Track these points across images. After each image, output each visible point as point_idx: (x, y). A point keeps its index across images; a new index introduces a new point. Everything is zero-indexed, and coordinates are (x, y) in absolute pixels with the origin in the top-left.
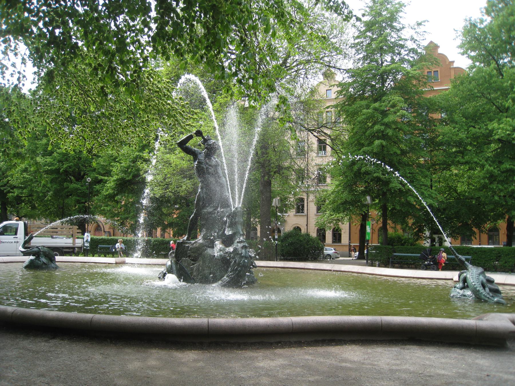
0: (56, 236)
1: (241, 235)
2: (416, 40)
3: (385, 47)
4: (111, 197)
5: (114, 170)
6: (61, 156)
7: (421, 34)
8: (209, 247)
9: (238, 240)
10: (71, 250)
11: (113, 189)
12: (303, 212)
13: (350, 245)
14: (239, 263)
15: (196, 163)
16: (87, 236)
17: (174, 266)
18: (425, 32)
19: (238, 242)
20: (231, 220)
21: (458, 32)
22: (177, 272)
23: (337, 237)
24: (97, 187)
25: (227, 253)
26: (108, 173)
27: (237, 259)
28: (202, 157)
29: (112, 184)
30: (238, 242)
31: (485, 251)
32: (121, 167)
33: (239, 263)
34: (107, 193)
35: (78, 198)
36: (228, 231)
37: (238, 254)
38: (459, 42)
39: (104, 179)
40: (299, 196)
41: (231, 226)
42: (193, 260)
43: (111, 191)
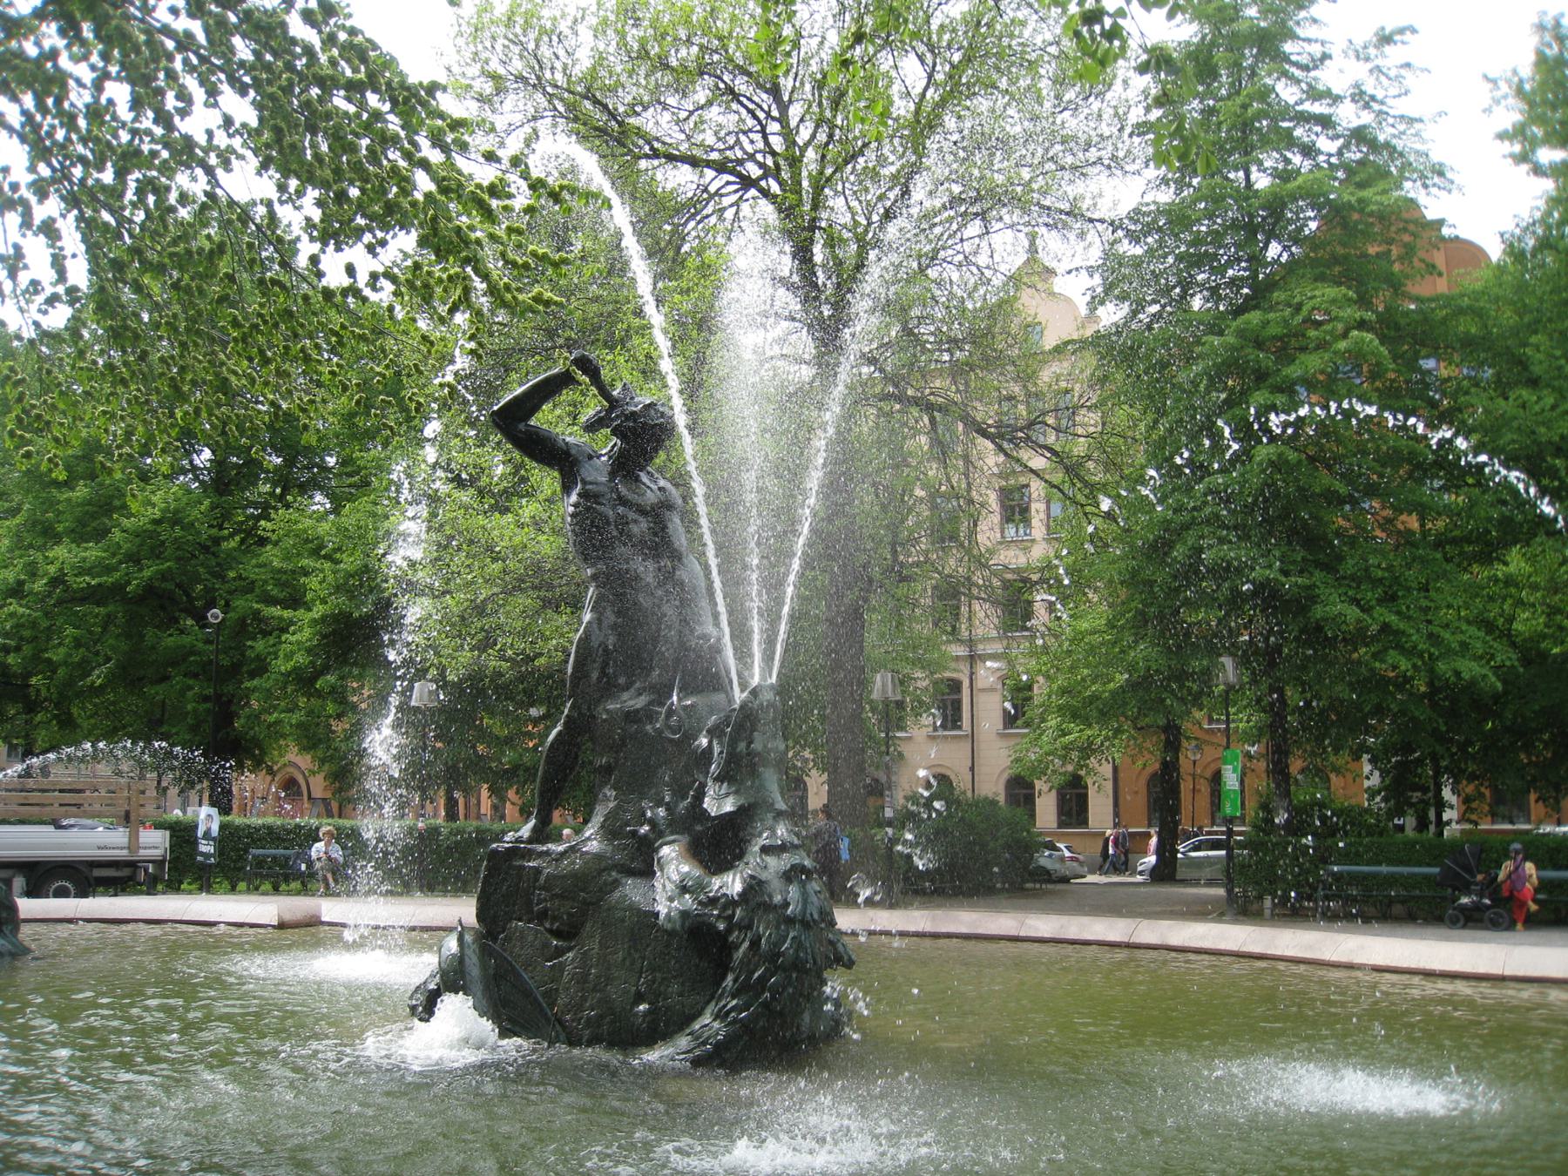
0: (72, 821)
1: (779, 814)
2: (1373, 98)
3: (1253, 128)
5: (313, 582)
7: (1392, 73)
8: (632, 873)
9: (764, 839)
11: (309, 651)
12: (960, 728)
14: (774, 955)
15: (574, 498)
17: (473, 961)
18: (1408, 65)
19: (765, 850)
20: (733, 742)
22: (487, 989)
23: (1073, 807)
25: (713, 901)
27: (765, 931)
28: (597, 472)
29: (307, 633)
30: (765, 850)
33: (774, 955)
34: (290, 665)
36: (720, 798)
37: (768, 907)
40: (947, 674)
42: (558, 934)
43: (301, 659)
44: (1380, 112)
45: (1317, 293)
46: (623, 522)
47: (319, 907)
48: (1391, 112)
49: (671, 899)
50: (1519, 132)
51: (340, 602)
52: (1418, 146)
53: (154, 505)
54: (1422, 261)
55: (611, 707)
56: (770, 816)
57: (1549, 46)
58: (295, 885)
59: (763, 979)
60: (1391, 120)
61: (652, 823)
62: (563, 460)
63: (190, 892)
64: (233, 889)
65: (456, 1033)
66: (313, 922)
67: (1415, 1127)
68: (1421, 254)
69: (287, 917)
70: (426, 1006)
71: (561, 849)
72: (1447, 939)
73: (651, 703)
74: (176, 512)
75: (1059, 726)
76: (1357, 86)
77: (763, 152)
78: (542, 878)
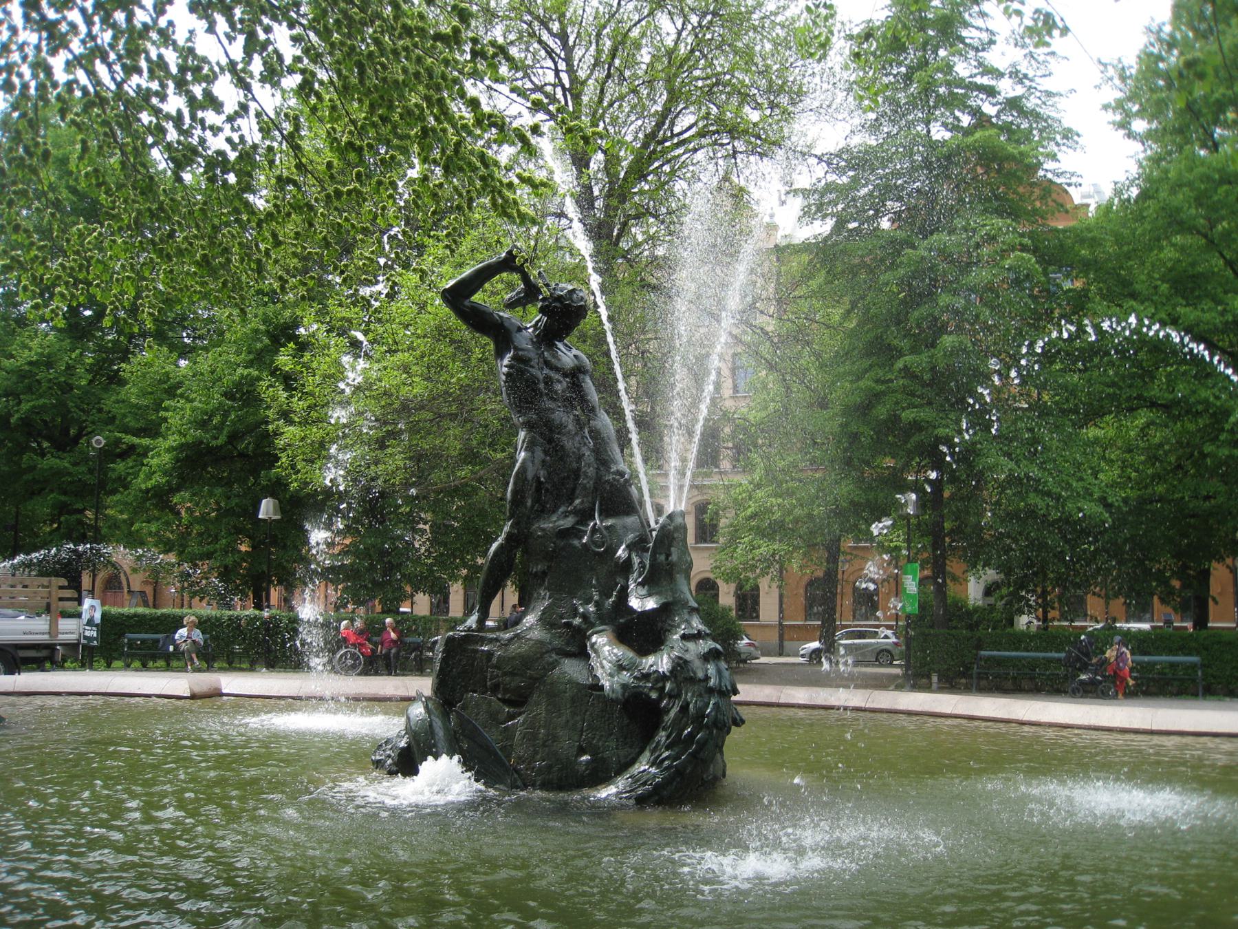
2: (1025, 76)
3: (936, 93)
4: (160, 498)
6: (14, 378)
7: (1041, 59)
10: (44, 653)
11: (165, 473)
13: (780, 624)
15: (506, 362)
16: (91, 607)
17: (438, 724)
21: (1110, 68)
24: (120, 467)
25: (646, 677)
26: (153, 430)
29: (167, 458)
31: (1230, 643)
32: (193, 410)
33: (701, 715)
34: (150, 484)
35: (63, 498)
37: (693, 680)
38: (1112, 94)
39: (140, 445)
41: (651, 582)
43: (158, 479)
44: (1030, 87)
45: (987, 222)
46: (548, 381)
47: (219, 681)
48: (1039, 88)
49: (611, 675)
50: (1119, 105)
51: (195, 434)
52: (1053, 114)
53: (30, 349)
54: (1054, 201)
57: (1152, 45)
58: (161, 663)
59: (691, 736)
60: (1038, 94)
61: (585, 617)
62: (501, 335)
63: (74, 669)
64: (108, 666)
65: (444, 780)
66: (217, 694)
67: (1155, 837)
68: (1054, 196)
69: (197, 690)
72: (1171, 707)
74: (49, 356)
76: (1014, 65)
77: (554, 86)
78: (494, 660)
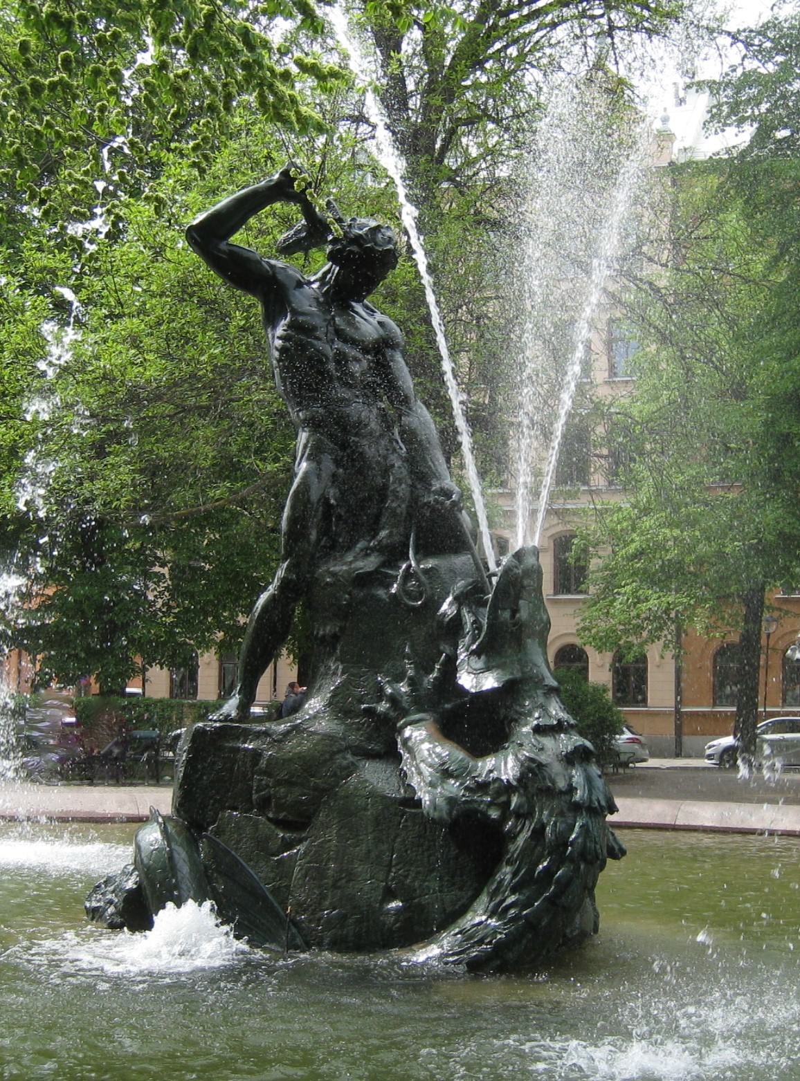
13: (677, 711)
15: (280, 331)
17: (181, 855)
19: (538, 730)
25: (483, 787)
28: (307, 298)
33: (562, 842)
37: (550, 792)
41: (492, 649)
46: (341, 359)
49: (432, 785)
55: (337, 569)
56: (540, 692)
61: (394, 700)
62: (272, 292)
65: (189, 936)
70: (136, 913)
71: (282, 727)
73: (383, 565)
75: (635, 591)
78: (263, 763)
